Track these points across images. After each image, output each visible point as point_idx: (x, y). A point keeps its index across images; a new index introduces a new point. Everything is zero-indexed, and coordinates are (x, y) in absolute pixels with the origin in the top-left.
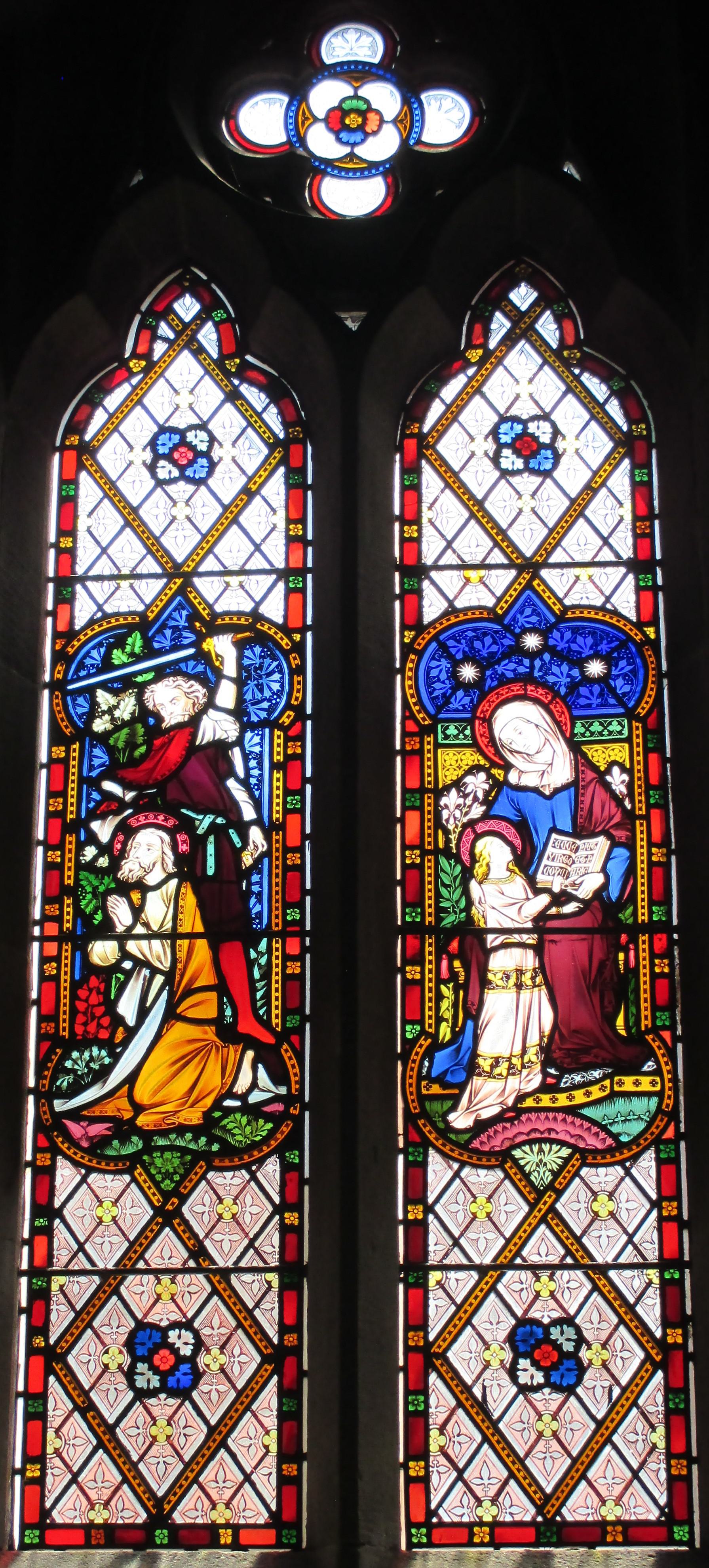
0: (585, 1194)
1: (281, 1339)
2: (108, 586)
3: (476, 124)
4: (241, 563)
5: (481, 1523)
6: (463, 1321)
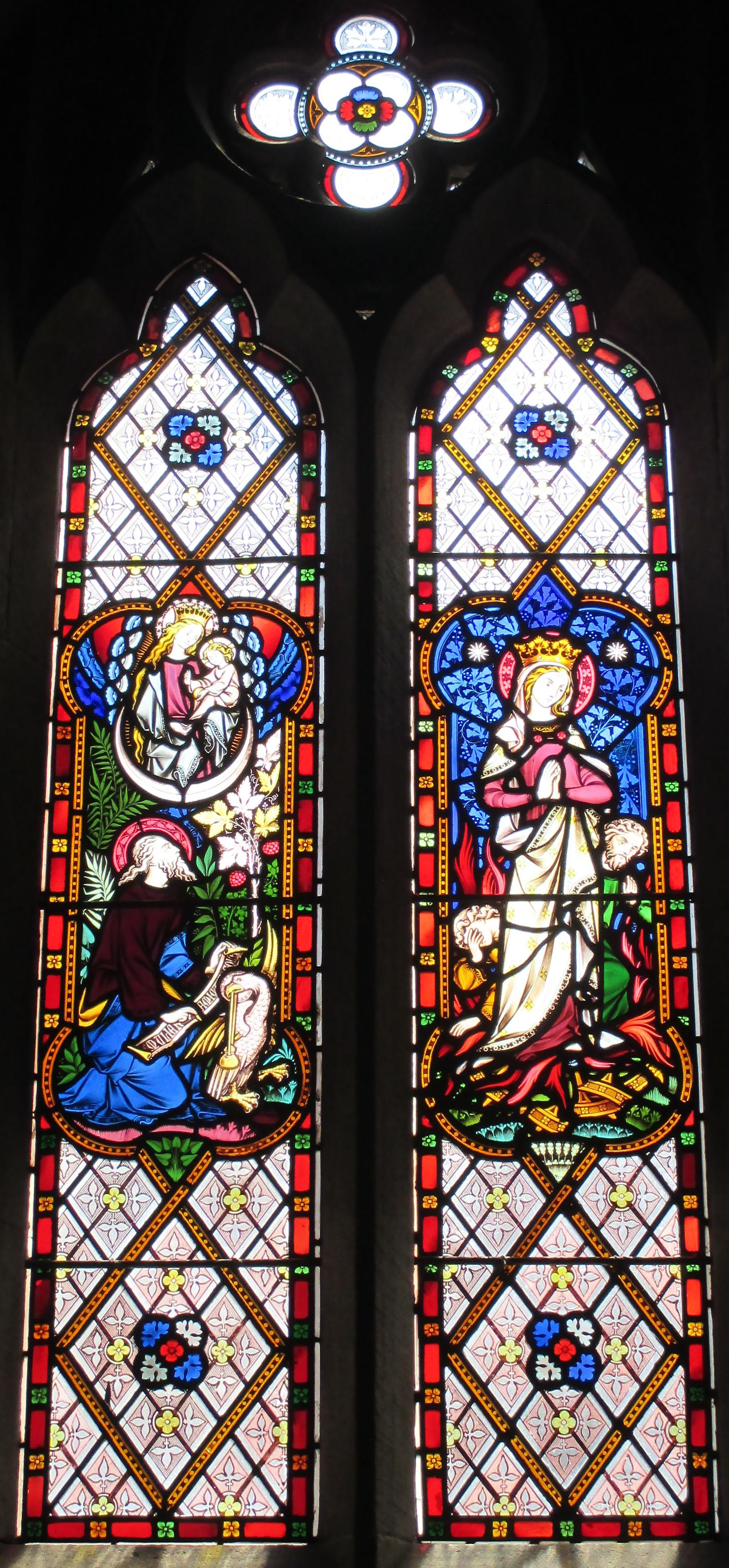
0: (603, 1185)
1: (686, 1329)
2: (119, 573)
3: (488, 118)
4: (253, 549)
5: (498, 1518)
6: (87, 1317)
